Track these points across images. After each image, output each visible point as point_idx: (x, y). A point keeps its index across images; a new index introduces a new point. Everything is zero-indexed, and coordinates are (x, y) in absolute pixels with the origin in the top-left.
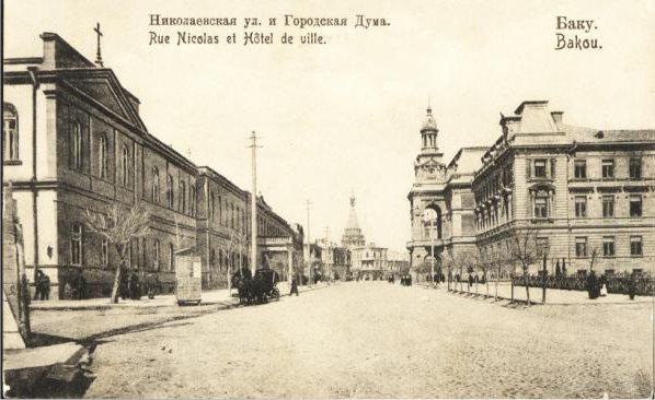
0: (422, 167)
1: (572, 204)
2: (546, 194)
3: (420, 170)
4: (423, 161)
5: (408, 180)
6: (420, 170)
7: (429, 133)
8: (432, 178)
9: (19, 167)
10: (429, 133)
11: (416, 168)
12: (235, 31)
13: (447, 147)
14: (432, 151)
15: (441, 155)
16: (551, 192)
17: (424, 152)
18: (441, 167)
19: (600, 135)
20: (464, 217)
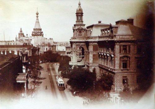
0: (77, 30)
1: (42, 30)
2: (127, 59)
3: (76, 31)
4: (77, 28)
5: (19, 32)
6: (76, 31)
7: (80, 14)
8: (81, 35)
9: (46, 79)
10: (80, 14)
11: (74, 30)
12: (47, 79)
13: (87, 21)
14: (80, 23)
15: (84, 25)
16: (128, 59)
17: (78, 23)
18: (84, 30)
19: (100, 22)
20: (94, 55)
